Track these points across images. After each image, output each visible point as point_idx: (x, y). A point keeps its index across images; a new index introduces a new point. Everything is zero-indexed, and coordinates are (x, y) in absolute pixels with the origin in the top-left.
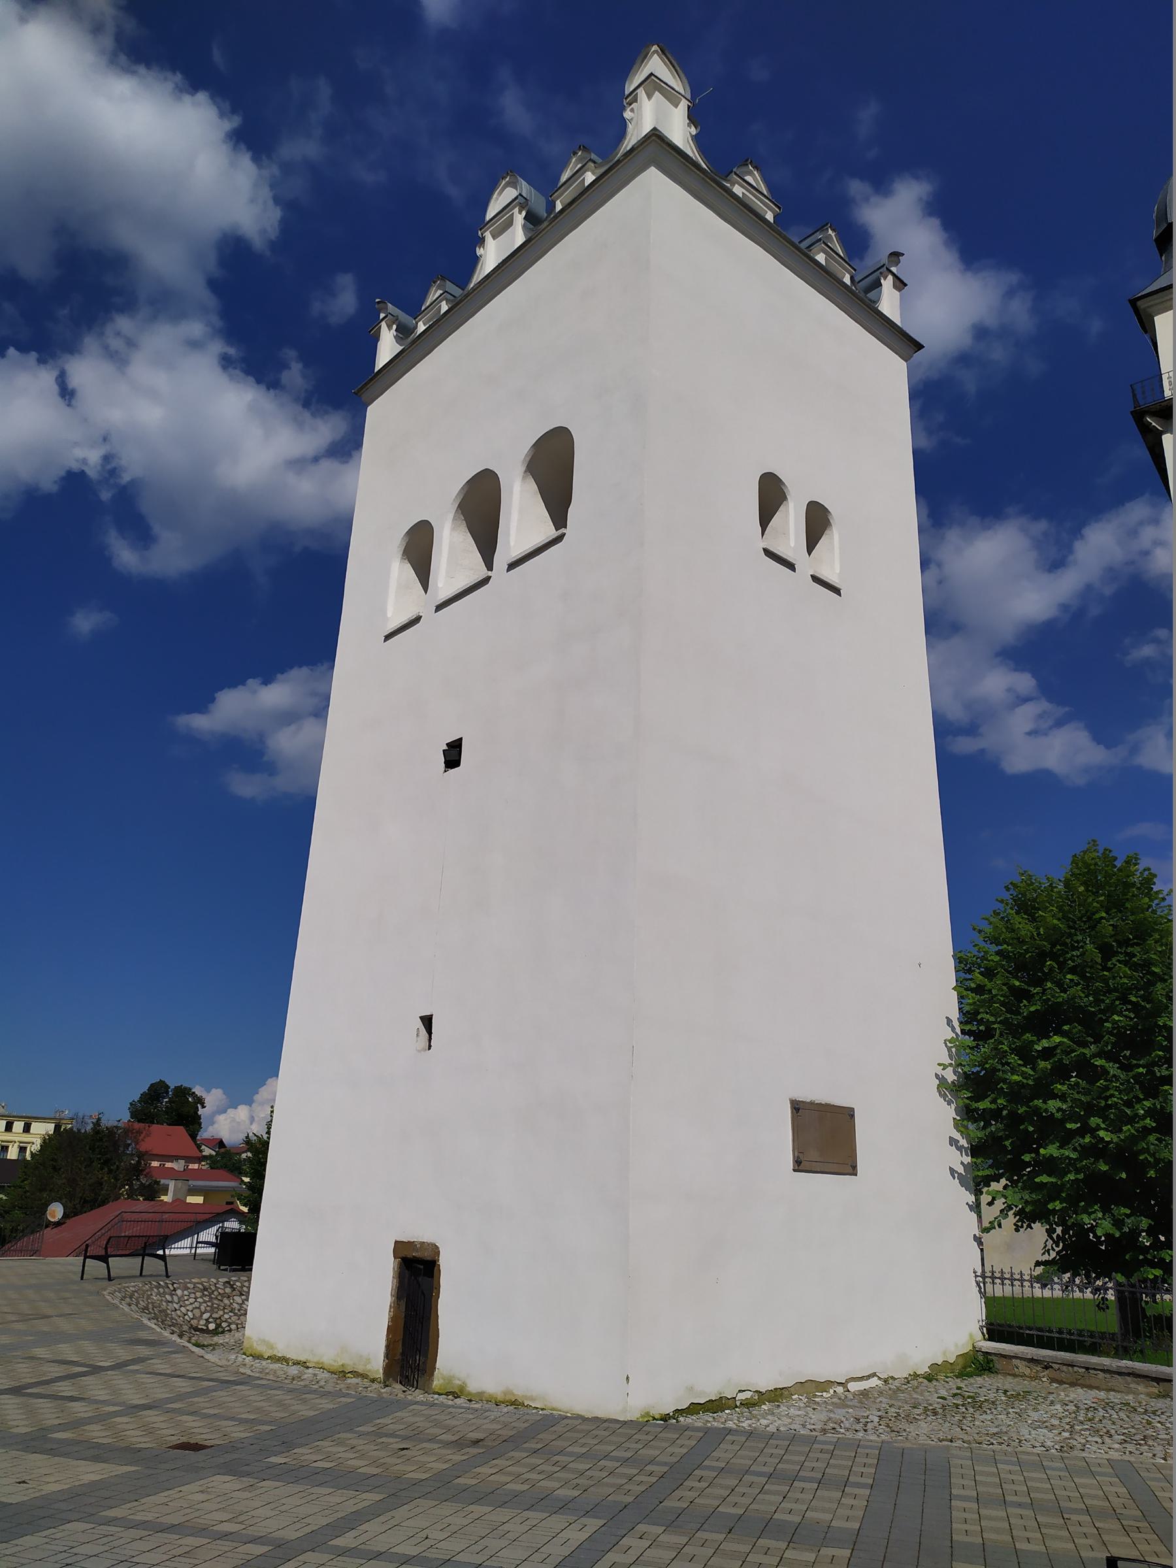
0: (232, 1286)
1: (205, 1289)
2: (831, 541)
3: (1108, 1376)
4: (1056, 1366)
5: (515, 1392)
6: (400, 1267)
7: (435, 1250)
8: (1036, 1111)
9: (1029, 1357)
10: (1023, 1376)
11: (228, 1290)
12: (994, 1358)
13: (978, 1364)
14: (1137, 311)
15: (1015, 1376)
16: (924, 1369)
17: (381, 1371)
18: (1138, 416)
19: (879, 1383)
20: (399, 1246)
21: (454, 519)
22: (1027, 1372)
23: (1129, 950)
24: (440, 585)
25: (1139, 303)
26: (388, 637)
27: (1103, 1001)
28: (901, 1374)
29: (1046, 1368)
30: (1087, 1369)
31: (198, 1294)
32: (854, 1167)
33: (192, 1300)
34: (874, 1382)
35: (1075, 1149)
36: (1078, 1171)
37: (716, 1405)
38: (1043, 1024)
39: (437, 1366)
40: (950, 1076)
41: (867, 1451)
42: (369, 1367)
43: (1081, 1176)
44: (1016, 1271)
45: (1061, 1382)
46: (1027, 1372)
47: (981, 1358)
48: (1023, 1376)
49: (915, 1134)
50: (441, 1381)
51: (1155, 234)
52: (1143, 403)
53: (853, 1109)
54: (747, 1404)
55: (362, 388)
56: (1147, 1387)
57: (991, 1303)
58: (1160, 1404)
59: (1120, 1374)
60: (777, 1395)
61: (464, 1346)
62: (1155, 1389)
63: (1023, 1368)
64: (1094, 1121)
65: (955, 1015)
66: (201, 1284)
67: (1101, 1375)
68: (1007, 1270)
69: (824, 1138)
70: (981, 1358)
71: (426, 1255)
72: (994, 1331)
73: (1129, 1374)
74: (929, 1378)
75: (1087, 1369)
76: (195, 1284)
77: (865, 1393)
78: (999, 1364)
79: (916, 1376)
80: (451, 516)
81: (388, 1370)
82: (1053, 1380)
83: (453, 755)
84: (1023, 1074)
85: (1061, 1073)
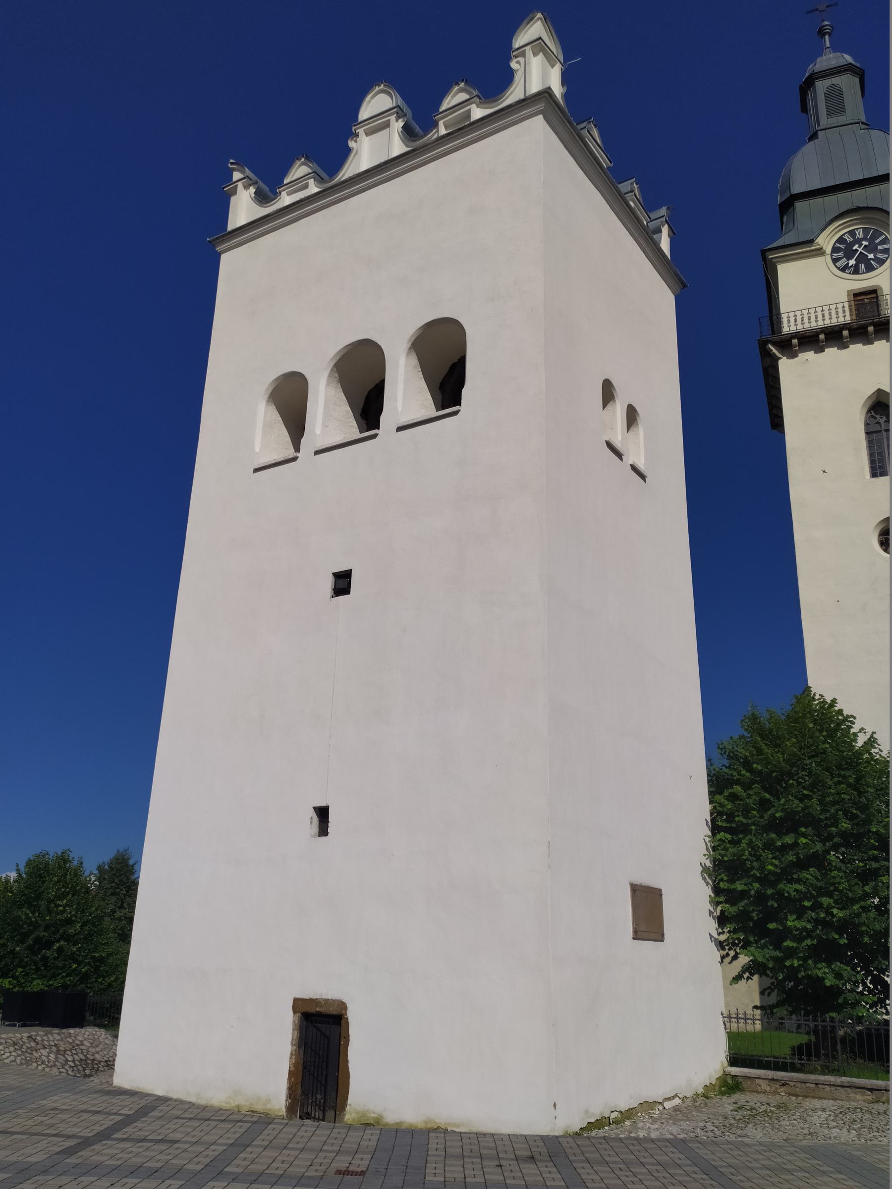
0: (35, 1040)
1: (15, 1044)
2: (641, 430)
3: (833, 1088)
4: (792, 1084)
5: (437, 1120)
6: (301, 1021)
7: (343, 1006)
8: (780, 894)
9: (770, 1077)
10: (765, 1092)
11: (33, 1044)
12: (740, 1080)
13: (729, 1086)
14: (764, 258)
15: (757, 1092)
16: (701, 1090)
17: (284, 1109)
18: (763, 345)
19: (680, 1101)
20: (298, 1004)
21: (330, 376)
22: (768, 1088)
23: (842, 773)
24: (318, 431)
25: (767, 254)
26: (256, 470)
27: (828, 811)
28: (690, 1094)
29: (783, 1085)
30: (817, 1084)
31: (12, 1049)
32: (663, 935)
33: (7, 1054)
34: (677, 1101)
35: (809, 921)
36: (812, 938)
37: (599, 1123)
38: (790, 823)
39: (349, 1101)
40: (708, 864)
41: (437, 1153)
42: (269, 1106)
43: (815, 942)
44: (741, 1012)
45: (797, 1096)
46: (768, 1088)
47: (730, 1081)
48: (765, 1092)
49: (691, 907)
50: (354, 1115)
51: (779, 200)
52: (767, 335)
53: (661, 890)
54: (617, 1122)
55: (217, 238)
56: (863, 1095)
57: (732, 1037)
58: (881, 1107)
59: (843, 1087)
60: (629, 1114)
61: (377, 1085)
62: (869, 1096)
63: (765, 1086)
64: (825, 901)
65: (709, 820)
66: (10, 1039)
67: (828, 1088)
68: (733, 1011)
69: (648, 913)
70: (730, 1081)
71: (333, 1010)
72: (734, 1061)
73: (849, 1087)
74: (706, 1096)
75: (817, 1084)
76: (5, 1039)
77: (676, 1109)
78: (746, 1084)
79: (697, 1094)
80: (327, 373)
81: (291, 1109)
82: (790, 1094)
83: (342, 583)
84: (776, 866)
85: (802, 864)
